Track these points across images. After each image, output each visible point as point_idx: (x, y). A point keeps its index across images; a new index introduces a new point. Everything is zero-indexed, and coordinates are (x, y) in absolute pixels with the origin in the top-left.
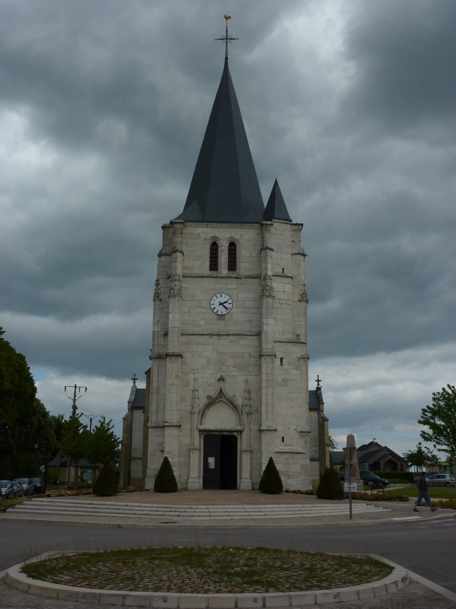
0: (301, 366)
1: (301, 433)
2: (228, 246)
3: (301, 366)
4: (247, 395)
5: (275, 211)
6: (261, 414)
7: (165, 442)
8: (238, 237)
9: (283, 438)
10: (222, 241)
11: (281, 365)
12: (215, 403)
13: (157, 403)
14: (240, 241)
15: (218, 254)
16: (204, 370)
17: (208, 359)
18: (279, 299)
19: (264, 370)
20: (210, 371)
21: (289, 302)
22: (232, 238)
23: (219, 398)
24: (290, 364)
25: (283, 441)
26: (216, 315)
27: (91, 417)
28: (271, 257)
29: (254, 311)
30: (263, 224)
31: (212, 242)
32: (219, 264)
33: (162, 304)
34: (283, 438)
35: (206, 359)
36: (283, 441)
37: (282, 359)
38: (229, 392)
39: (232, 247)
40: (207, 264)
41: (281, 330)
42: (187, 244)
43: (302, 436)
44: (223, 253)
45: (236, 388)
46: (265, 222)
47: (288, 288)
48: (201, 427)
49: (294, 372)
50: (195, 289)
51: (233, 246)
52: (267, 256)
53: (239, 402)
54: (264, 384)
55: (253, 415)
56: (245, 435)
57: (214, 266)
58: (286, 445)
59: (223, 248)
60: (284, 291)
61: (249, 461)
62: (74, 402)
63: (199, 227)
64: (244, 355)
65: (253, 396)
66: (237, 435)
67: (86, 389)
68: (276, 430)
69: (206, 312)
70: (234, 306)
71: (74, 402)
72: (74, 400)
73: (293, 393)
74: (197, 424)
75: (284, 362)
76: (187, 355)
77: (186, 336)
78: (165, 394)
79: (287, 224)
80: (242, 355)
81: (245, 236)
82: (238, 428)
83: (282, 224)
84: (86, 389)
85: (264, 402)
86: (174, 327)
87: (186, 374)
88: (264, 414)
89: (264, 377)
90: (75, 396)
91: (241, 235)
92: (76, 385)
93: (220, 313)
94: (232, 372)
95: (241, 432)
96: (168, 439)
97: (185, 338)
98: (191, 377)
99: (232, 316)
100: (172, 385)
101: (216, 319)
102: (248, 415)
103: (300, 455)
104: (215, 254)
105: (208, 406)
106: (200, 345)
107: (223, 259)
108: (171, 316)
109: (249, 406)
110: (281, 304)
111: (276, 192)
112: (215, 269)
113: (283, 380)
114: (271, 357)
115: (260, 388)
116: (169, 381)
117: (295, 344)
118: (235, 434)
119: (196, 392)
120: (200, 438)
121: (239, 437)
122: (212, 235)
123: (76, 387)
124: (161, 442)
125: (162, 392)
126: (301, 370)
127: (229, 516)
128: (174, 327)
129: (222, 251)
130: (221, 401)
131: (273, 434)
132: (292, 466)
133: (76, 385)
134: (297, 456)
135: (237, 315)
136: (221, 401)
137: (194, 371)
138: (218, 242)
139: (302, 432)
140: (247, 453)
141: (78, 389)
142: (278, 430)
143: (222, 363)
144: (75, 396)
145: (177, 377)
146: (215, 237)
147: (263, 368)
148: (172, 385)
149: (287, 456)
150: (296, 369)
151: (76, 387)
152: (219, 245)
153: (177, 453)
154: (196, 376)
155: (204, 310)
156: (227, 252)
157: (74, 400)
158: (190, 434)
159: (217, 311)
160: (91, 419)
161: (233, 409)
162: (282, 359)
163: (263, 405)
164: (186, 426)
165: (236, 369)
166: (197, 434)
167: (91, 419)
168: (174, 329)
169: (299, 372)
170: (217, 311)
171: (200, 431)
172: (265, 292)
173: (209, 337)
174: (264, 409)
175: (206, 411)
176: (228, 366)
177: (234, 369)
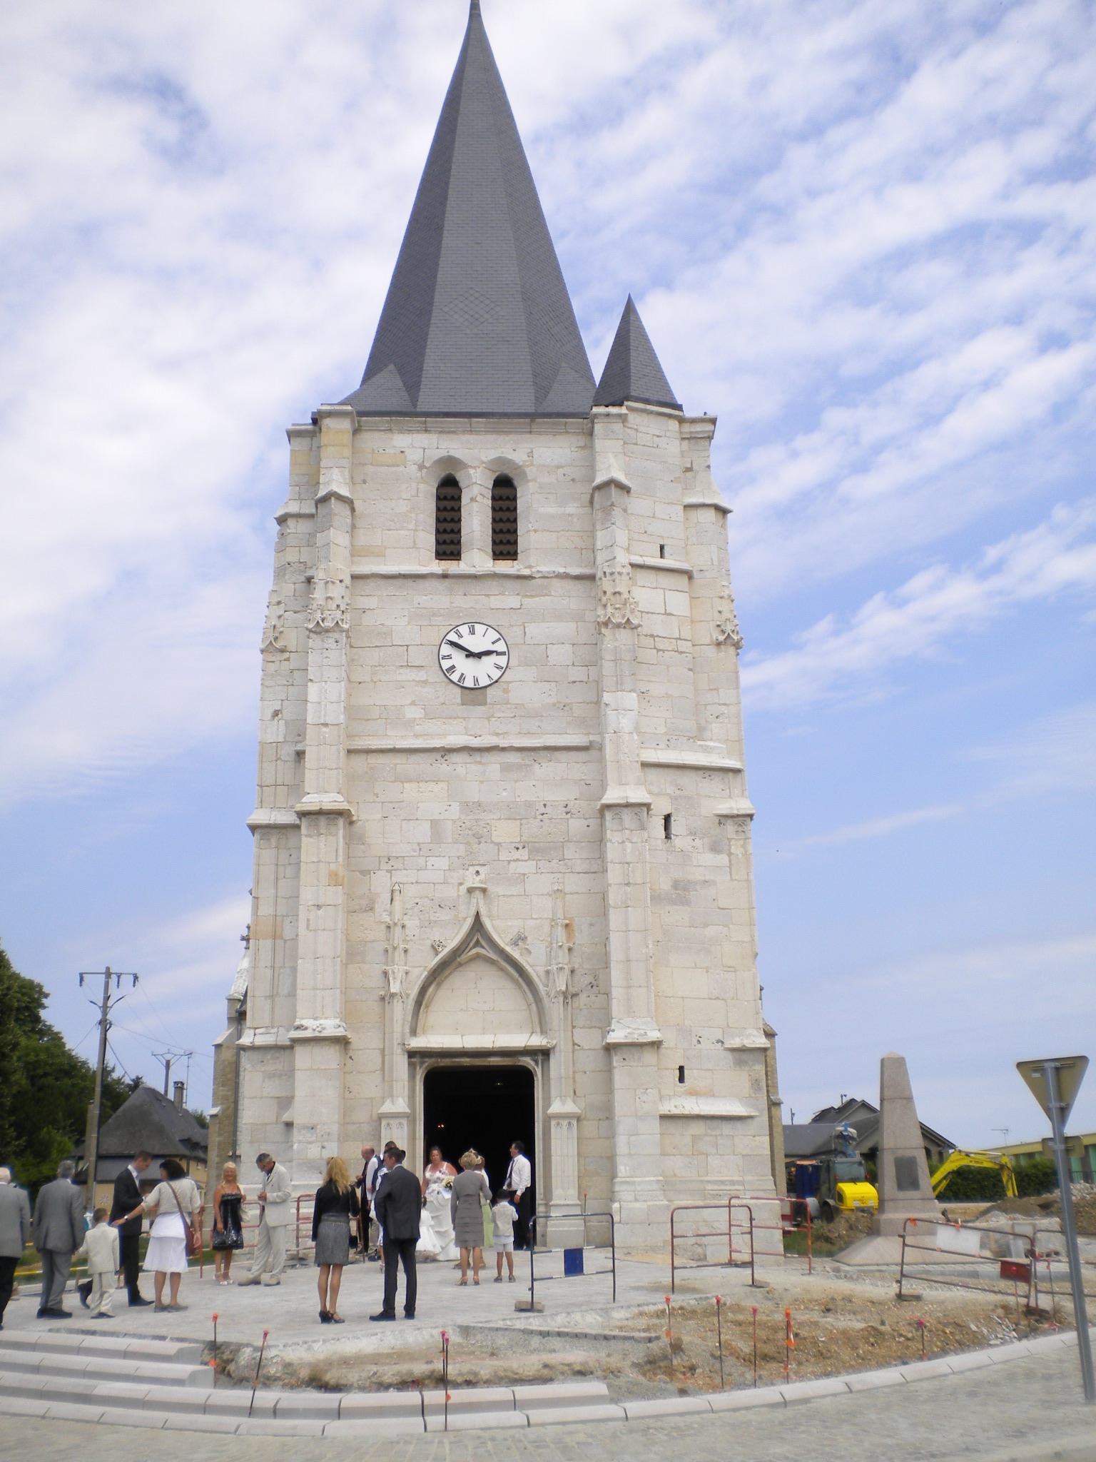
0: (730, 840)
1: (736, 1054)
2: (491, 486)
3: (730, 840)
4: (561, 934)
5: (631, 377)
6: (608, 994)
7: (297, 1093)
8: (519, 457)
9: (681, 1069)
10: (471, 471)
11: (668, 837)
12: (460, 965)
13: (273, 967)
14: (527, 470)
15: (459, 510)
16: (422, 861)
17: (434, 823)
18: (652, 636)
19: (612, 852)
20: (443, 863)
21: (683, 646)
22: (501, 461)
23: (476, 947)
24: (693, 834)
25: (681, 1079)
26: (458, 691)
27: (168, 1057)
28: (625, 510)
29: (578, 673)
30: (596, 416)
31: (443, 474)
32: (463, 540)
33: (288, 660)
34: (681, 1069)
35: (427, 826)
36: (681, 1079)
37: (667, 818)
38: (500, 930)
39: (504, 491)
40: (428, 539)
41: (662, 730)
42: (364, 482)
43: (740, 1063)
44: (475, 504)
45: (526, 915)
46: (602, 410)
47: (679, 602)
48: (418, 1043)
49: (709, 859)
50: (394, 615)
51: (505, 490)
52: (612, 505)
53: (534, 964)
54: (613, 898)
55: (583, 997)
56: (557, 1064)
57: (449, 546)
58: (693, 1093)
59: (476, 490)
60: (666, 614)
61: (572, 1149)
62: (105, 1013)
63: (401, 431)
64: (548, 810)
65: (582, 937)
66: (533, 1063)
67: (136, 978)
68: (656, 1045)
69: (425, 682)
70: (513, 662)
71: (105, 1013)
72: (105, 1009)
73: (706, 925)
74: (403, 1035)
75: (675, 827)
76: (368, 816)
77: (364, 756)
78: (296, 938)
79: (670, 416)
80: (542, 810)
81: (542, 458)
82: (537, 1041)
83: (652, 417)
84: (136, 978)
85: (616, 954)
86: (326, 725)
87: (365, 873)
88: (616, 993)
89: (614, 874)
90: (107, 998)
91: (530, 454)
92: (108, 969)
93: (469, 683)
94: (513, 864)
95: (544, 1054)
96: (303, 1085)
97: (360, 763)
98: (380, 883)
99: (506, 691)
100: (319, 907)
101: (459, 700)
102: (565, 998)
103: (738, 1124)
104: (453, 498)
105: (438, 974)
106: (410, 781)
107: (476, 519)
108: (313, 691)
109: (567, 972)
110: (658, 650)
111: (629, 336)
112: (452, 554)
113: (676, 884)
114: (637, 810)
115: (603, 912)
116: (308, 895)
117: (708, 773)
118: (527, 1061)
119: (398, 930)
120: (412, 1077)
121: (538, 1072)
122: (442, 453)
123: (108, 974)
124: (283, 1094)
125: (288, 934)
126: (730, 854)
127: (515, 1405)
128: (326, 725)
129: (472, 500)
130: (478, 957)
131: (649, 1057)
132: (714, 1161)
133: (108, 969)
134: (727, 1128)
135: (526, 689)
136: (478, 957)
137: (391, 863)
138: (460, 477)
139: (743, 1050)
140: (565, 1123)
141: (114, 977)
142: (665, 1045)
143: (479, 837)
144: (107, 998)
145: (334, 879)
146: (450, 461)
147: (609, 844)
148: (319, 907)
149: (697, 1128)
150: (715, 848)
151: (108, 974)
152: (462, 485)
153: (335, 1129)
154: (399, 876)
155: (422, 675)
156: (490, 502)
157: (105, 1009)
158: (378, 1066)
159: (462, 677)
160: (168, 1063)
161: (520, 987)
162: (667, 818)
163: (613, 965)
164: (366, 1043)
165: (523, 854)
166: (402, 1063)
167: (168, 1063)
168: (324, 729)
169: (723, 859)
170: (462, 677)
171: (412, 1054)
172: (608, 622)
173: (438, 756)
174: (616, 975)
175: (431, 990)
176: (498, 844)
177: (517, 855)
